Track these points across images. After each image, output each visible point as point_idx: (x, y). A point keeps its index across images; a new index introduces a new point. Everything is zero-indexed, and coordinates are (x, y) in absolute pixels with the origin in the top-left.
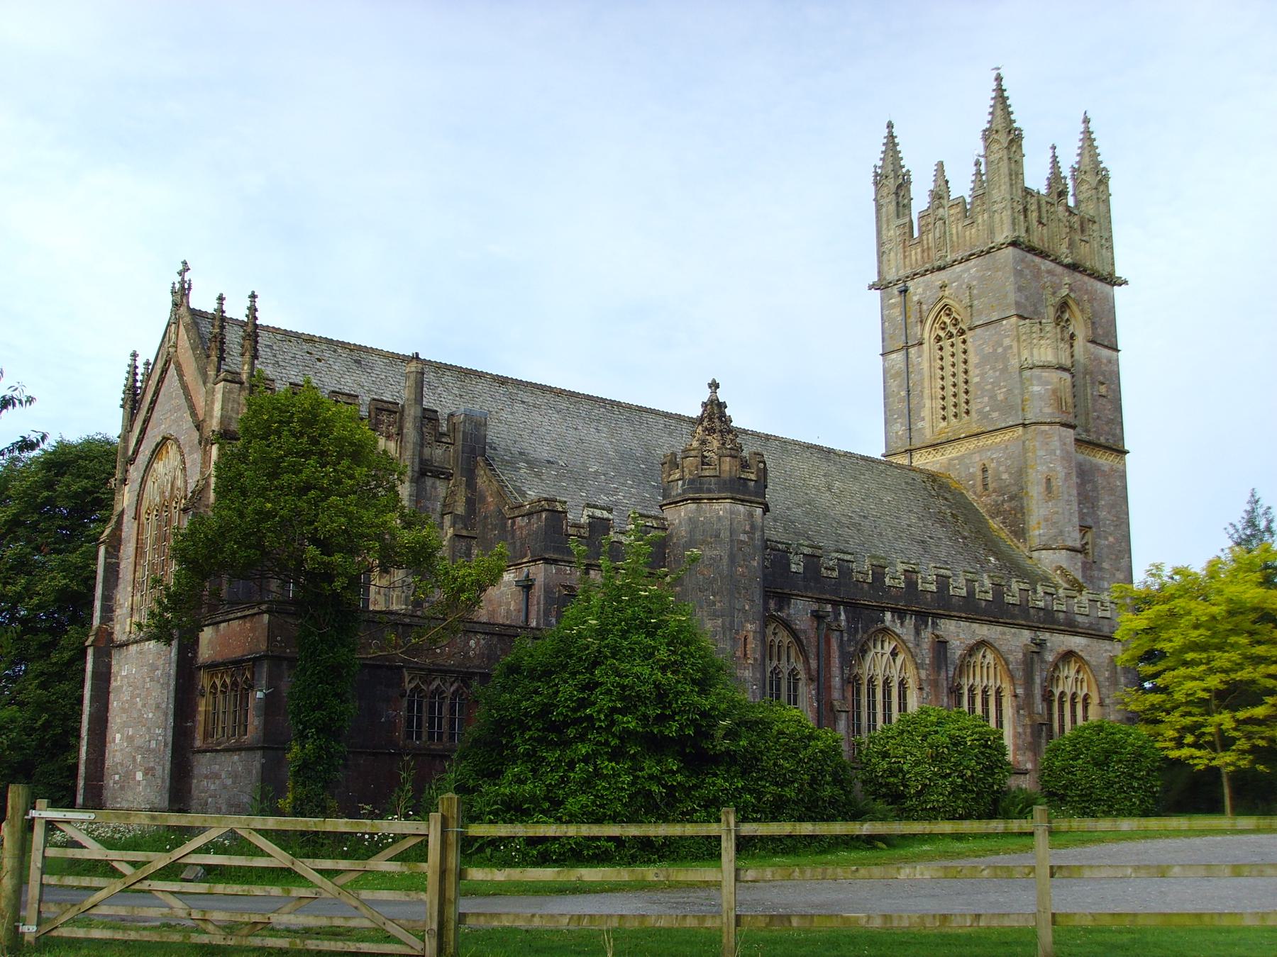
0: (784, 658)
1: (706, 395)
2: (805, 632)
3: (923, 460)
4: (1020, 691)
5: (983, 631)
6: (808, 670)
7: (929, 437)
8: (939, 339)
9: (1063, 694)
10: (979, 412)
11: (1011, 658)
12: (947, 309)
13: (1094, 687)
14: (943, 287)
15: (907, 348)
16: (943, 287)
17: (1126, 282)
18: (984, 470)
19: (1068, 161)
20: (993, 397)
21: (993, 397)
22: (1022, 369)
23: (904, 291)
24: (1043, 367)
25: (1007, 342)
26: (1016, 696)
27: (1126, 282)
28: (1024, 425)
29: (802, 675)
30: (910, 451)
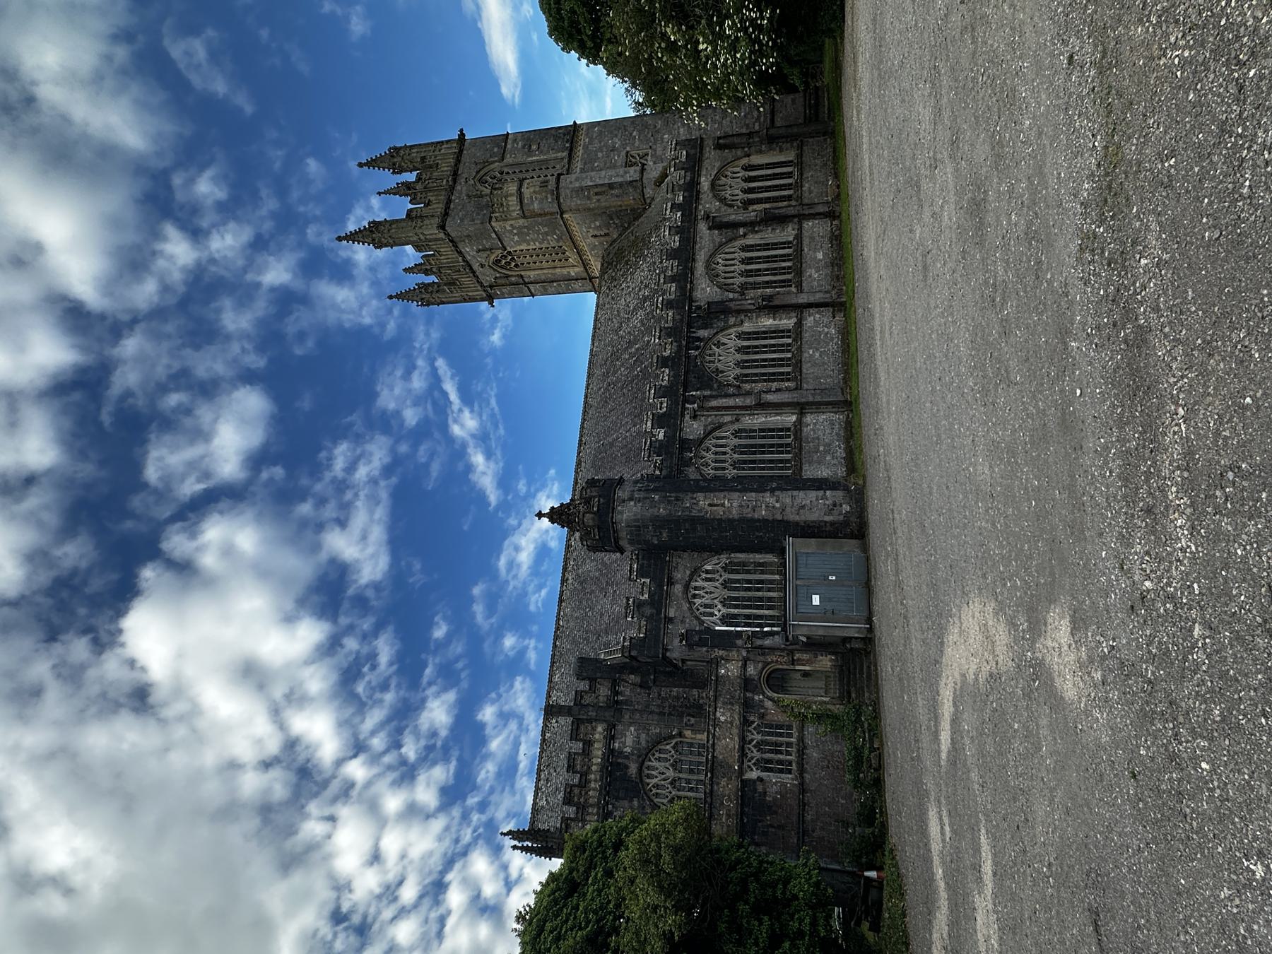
0: (732, 269)
1: (545, 520)
2: (706, 426)
3: (596, 267)
4: (741, 231)
5: (700, 266)
6: (732, 422)
7: (580, 269)
8: (516, 266)
9: (745, 191)
10: (558, 241)
11: (718, 240)
12: (497, 262)
13: (736, 163)
14: (482, 266)
15: (525, 283)
16: (482, 266)
17: (461, 131)
18: (595, 236)
19: (391, 179)
20: (546, 234)
21: (546, 234)
22: (524, 217)
23: (491, 287)
24: (521, 203)
25: (508, 228)
26: (745, 235)
27: (461, 131)
28: (562, 213)
29: (736, 427)
30: (591, 279)
